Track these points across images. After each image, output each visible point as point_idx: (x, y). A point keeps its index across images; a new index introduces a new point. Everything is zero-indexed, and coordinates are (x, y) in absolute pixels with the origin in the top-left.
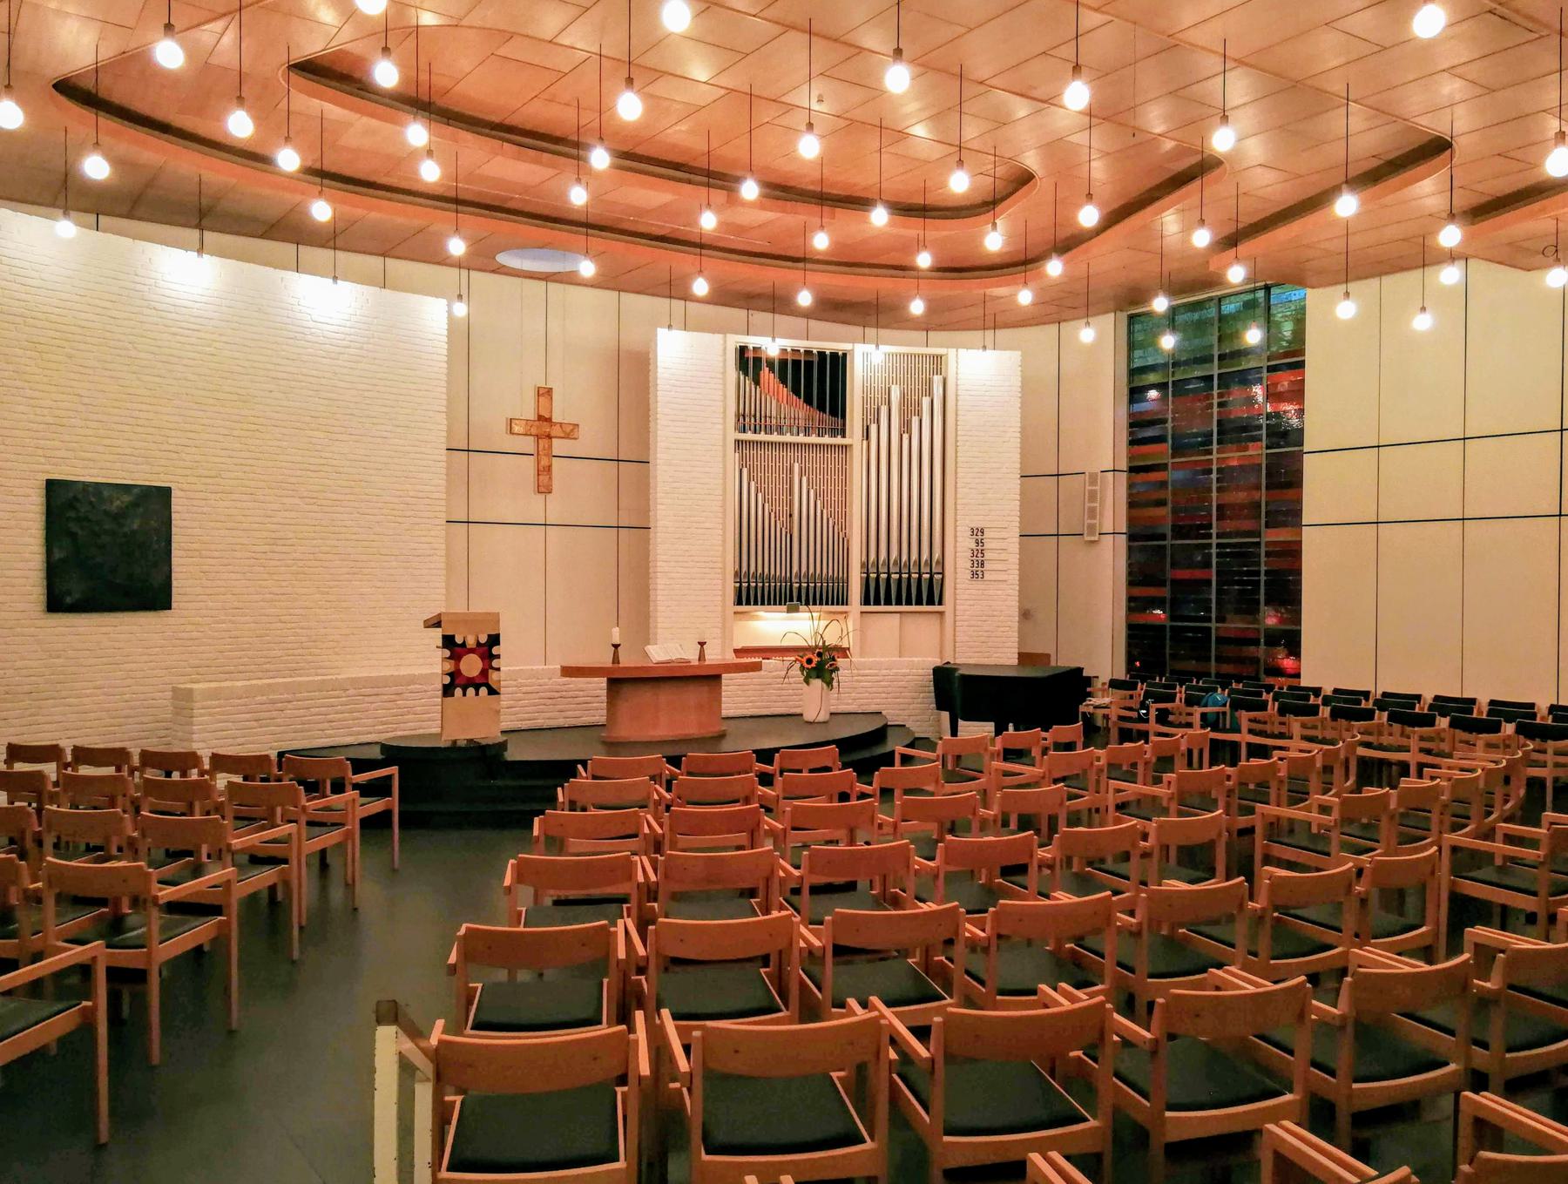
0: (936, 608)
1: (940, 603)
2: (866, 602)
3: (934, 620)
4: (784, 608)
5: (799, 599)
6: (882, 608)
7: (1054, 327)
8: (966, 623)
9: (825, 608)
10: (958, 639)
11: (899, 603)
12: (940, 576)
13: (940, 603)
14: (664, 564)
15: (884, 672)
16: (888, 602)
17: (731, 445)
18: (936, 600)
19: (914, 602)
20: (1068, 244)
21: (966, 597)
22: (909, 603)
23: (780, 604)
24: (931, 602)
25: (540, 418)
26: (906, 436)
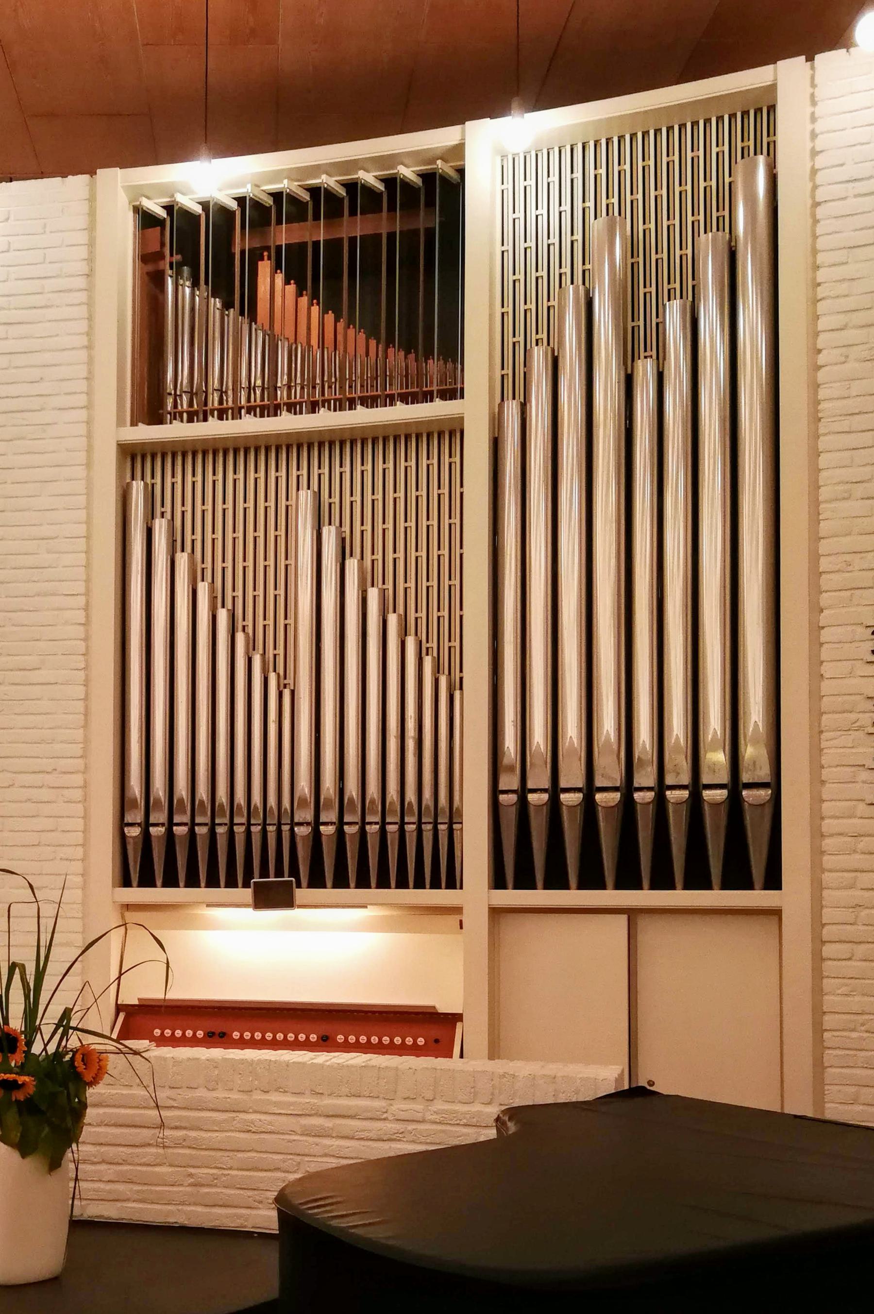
1: (773, 881)
3: (762, 928)
4: (247, 894)
5: (294, 871)
10: (830, 1001)
12: (765, 794)
15: (399, 1107)
19: (411, 884)
23: (231, 883)
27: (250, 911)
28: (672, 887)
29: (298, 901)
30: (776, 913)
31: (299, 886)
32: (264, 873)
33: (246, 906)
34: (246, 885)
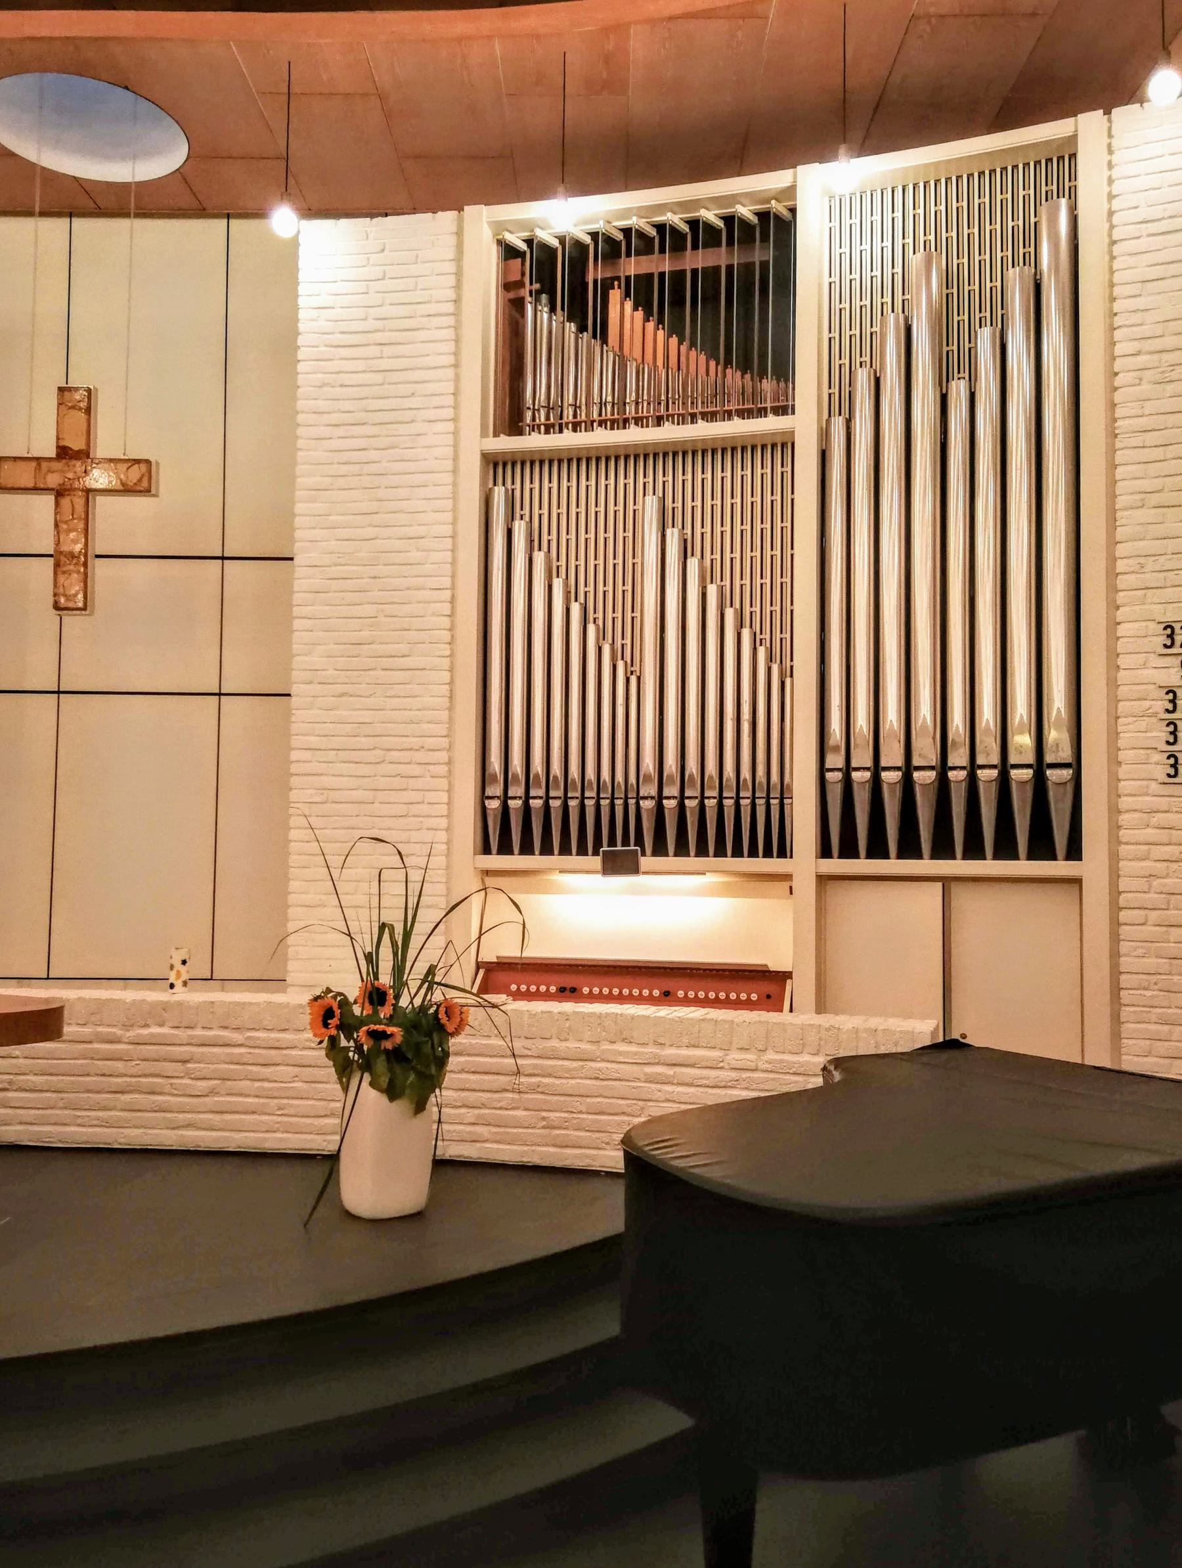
0: (1060, 868)
1: (1074, 852)
2: (825, 851)
3: (1061, 898)
4: (596, 862)
5: (639, 841)
6: (893, 866)
7: (64, 222)
8: (1154, 916)
9: (730, 862)
10: (1126, 962)
11: (942, 849)
12: (1067, 774)
13: (783, 853)
14: (307, 755)
15: (735, 1057)
16: (909, 849)
17: (472, 468)
18: (788, 854)
19: (775, 854)
20: (268, 51)
21: (1150, 834)
22: (974, 850)
23: (582, 851)
24: (1042, 848)
25: (64, 453)
26: (838, 424)
27: (599, 877)
28: (953, 857)
29: (643, 868)
30: (1077, 882)
31: (644, 854)
32: (612, 842)
33: (596, 872)
34: (596, 853)
